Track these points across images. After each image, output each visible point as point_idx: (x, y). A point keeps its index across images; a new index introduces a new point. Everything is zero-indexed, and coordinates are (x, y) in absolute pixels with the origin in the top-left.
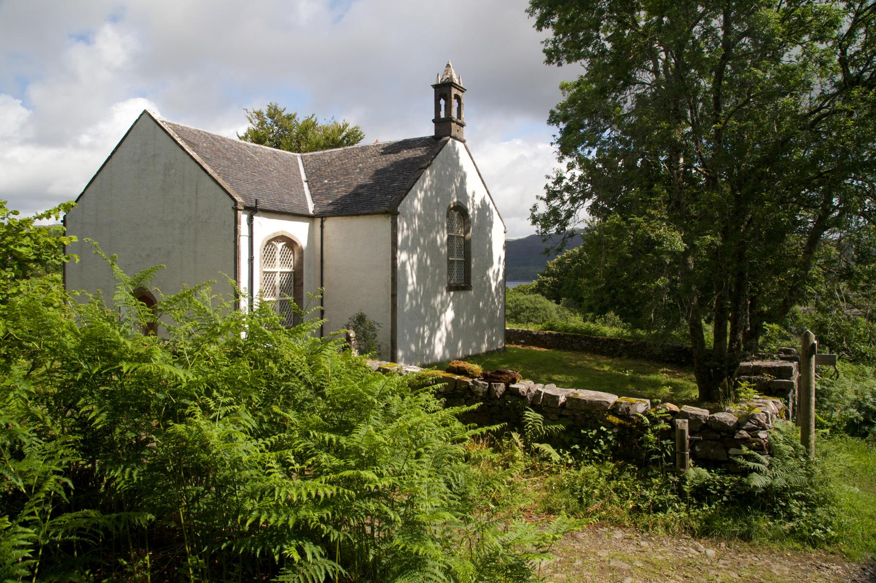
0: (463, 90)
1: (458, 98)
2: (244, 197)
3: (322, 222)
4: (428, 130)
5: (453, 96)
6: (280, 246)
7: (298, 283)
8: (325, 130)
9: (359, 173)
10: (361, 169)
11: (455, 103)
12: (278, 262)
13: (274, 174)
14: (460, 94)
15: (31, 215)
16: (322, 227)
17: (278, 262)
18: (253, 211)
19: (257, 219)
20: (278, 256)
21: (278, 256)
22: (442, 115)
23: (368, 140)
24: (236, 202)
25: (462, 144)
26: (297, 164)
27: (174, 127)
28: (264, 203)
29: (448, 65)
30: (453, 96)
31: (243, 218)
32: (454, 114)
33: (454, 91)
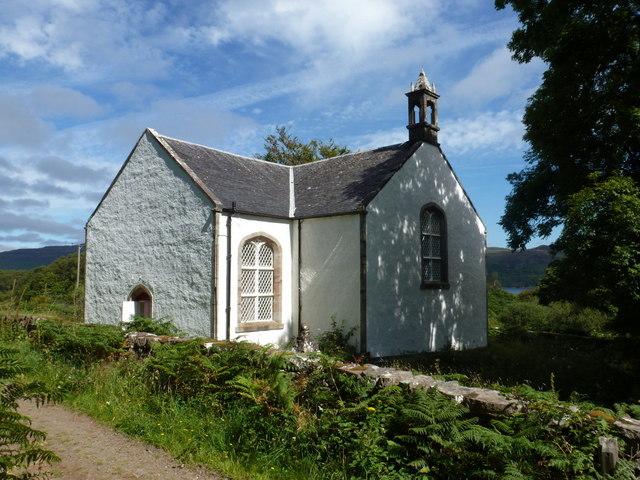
0: (436, 97)
1: (430, 104)
2: (223, 200)
3: (300, 224)
4: (402, 137)
5: (425, 103)
6: (259, 245)
7: (276, 280)
8: (27, 61)
9: (339, 179)
10: (341, 176)
11: (428, 110)
12: (257, 261)
13: (263, 182)
14: (433, 101)
15: (23, 415)
16: (229, 225)
17: (257, 261)
18: (230, 212)
19: (235, 220)
20: (257, 255)
21: (257, 255)
22: (417, 121)
23: (354, 152)
24: (214, 205)
25: (435, 149)
26: (288, 175)
27: (173, 145)
28: (241, 206)
29: (421, 74)
30: (425, 103)
31: (222, 219)
32: (428, 120)
33: (427, 98)
